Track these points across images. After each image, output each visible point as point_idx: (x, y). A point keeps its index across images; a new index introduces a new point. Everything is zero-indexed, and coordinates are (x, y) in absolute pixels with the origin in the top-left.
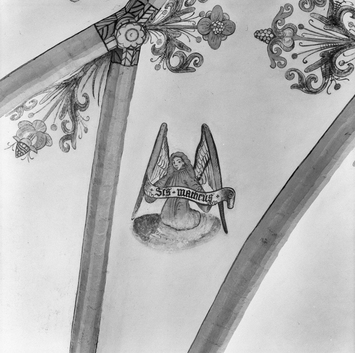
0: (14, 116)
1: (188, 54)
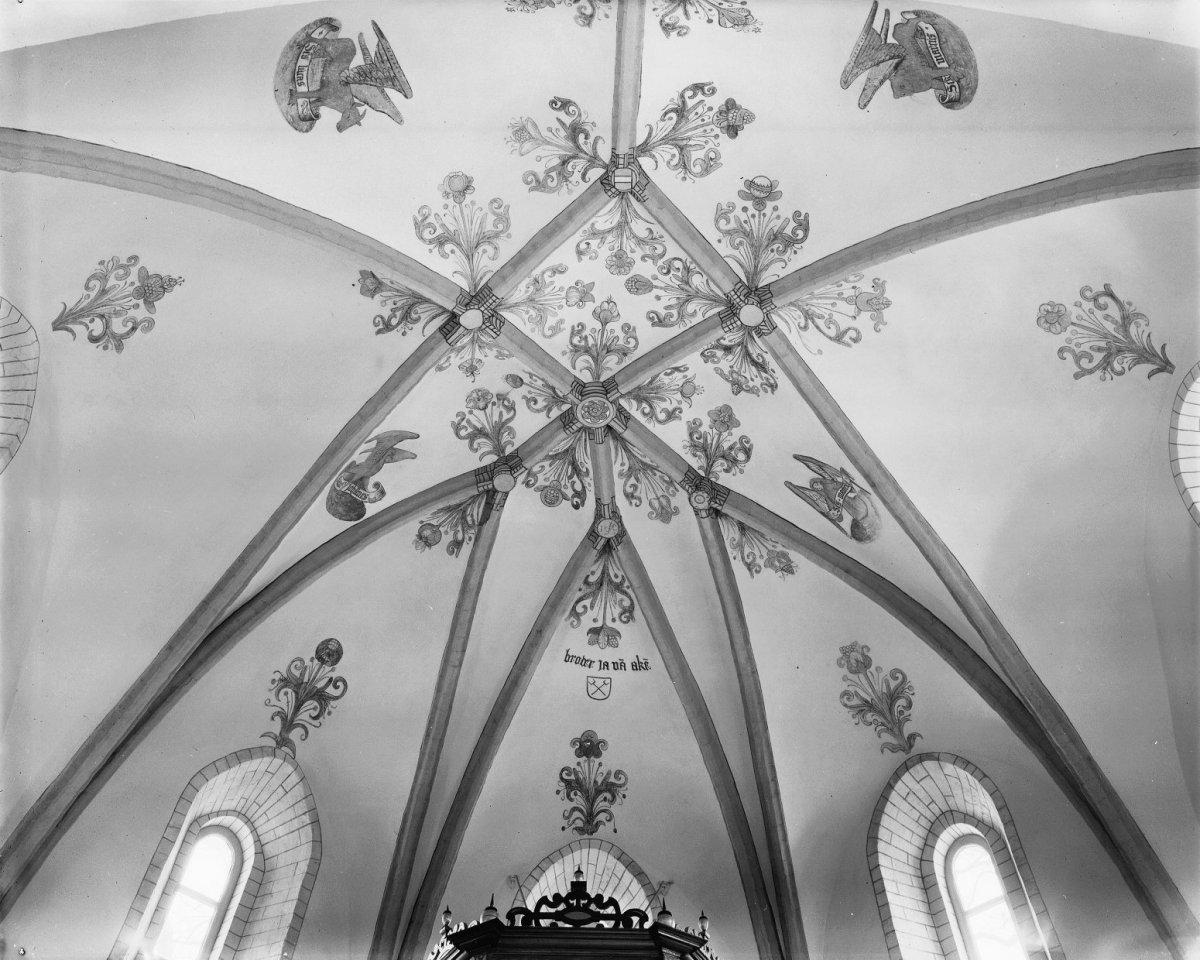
0: (756, 571)
1: (738, 445)
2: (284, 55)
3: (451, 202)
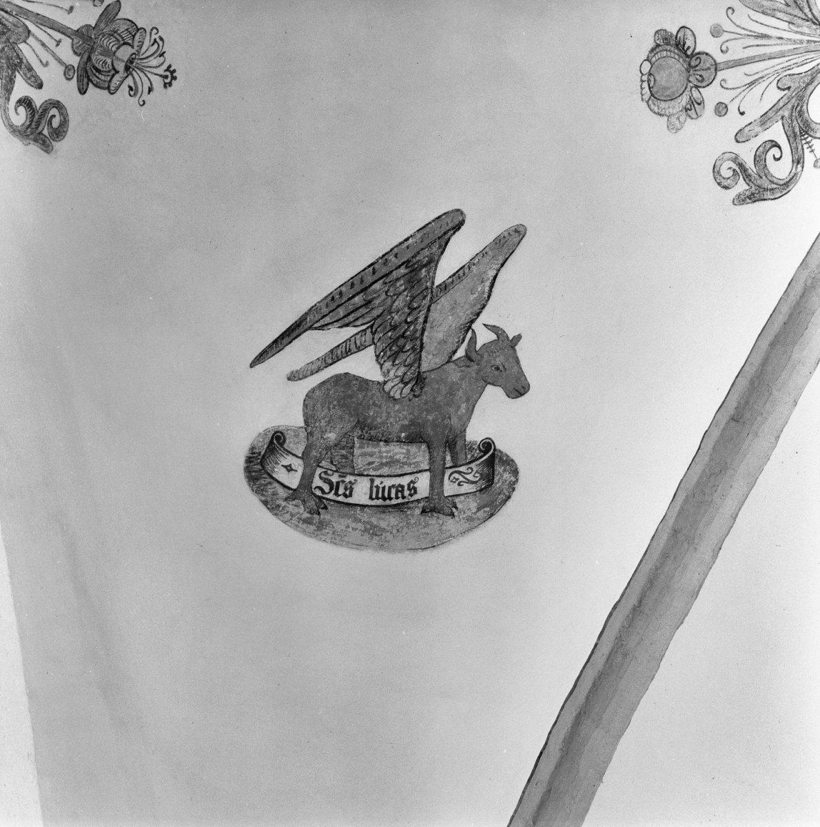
2: (338, 539)
3: (711, 95)
